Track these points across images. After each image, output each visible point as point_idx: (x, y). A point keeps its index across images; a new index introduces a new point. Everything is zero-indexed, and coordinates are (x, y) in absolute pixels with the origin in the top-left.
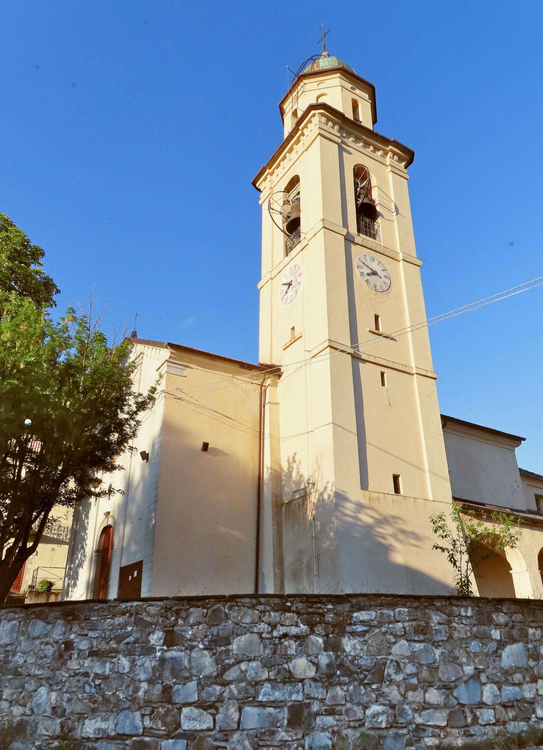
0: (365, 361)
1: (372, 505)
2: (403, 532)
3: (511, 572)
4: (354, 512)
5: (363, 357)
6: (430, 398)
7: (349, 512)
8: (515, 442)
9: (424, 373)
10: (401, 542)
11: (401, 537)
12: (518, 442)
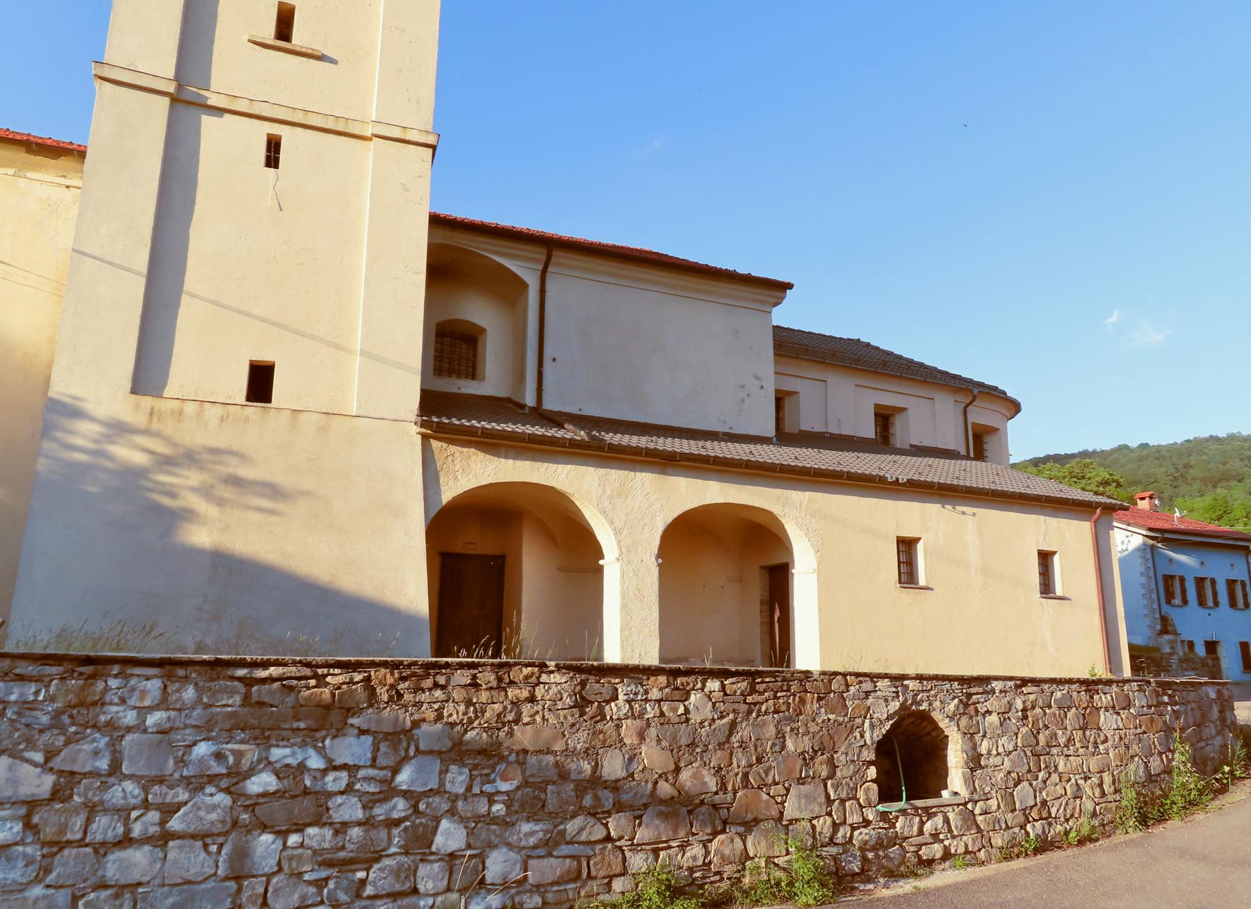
0: (220, 111)
1: (155, 426)
2: (236, 482)
3: (601, 562)
4: (96, 442)
5: (210, 102)
6: (407, 190)
7: (79, 442)
8: (768, 292)
9: (397, 133)
10: (221, 503)
11: (227, 492)
12: (780, 295)
